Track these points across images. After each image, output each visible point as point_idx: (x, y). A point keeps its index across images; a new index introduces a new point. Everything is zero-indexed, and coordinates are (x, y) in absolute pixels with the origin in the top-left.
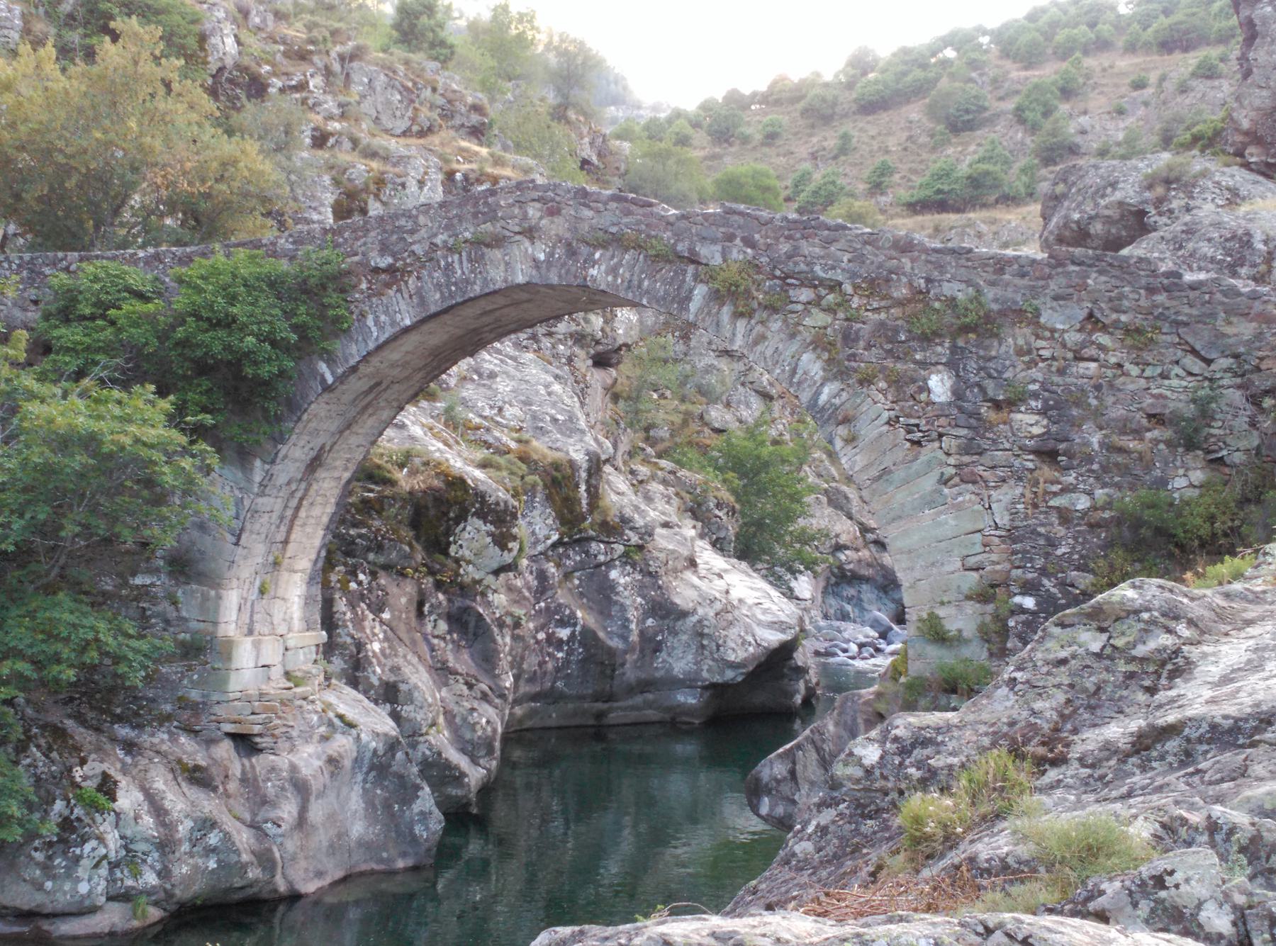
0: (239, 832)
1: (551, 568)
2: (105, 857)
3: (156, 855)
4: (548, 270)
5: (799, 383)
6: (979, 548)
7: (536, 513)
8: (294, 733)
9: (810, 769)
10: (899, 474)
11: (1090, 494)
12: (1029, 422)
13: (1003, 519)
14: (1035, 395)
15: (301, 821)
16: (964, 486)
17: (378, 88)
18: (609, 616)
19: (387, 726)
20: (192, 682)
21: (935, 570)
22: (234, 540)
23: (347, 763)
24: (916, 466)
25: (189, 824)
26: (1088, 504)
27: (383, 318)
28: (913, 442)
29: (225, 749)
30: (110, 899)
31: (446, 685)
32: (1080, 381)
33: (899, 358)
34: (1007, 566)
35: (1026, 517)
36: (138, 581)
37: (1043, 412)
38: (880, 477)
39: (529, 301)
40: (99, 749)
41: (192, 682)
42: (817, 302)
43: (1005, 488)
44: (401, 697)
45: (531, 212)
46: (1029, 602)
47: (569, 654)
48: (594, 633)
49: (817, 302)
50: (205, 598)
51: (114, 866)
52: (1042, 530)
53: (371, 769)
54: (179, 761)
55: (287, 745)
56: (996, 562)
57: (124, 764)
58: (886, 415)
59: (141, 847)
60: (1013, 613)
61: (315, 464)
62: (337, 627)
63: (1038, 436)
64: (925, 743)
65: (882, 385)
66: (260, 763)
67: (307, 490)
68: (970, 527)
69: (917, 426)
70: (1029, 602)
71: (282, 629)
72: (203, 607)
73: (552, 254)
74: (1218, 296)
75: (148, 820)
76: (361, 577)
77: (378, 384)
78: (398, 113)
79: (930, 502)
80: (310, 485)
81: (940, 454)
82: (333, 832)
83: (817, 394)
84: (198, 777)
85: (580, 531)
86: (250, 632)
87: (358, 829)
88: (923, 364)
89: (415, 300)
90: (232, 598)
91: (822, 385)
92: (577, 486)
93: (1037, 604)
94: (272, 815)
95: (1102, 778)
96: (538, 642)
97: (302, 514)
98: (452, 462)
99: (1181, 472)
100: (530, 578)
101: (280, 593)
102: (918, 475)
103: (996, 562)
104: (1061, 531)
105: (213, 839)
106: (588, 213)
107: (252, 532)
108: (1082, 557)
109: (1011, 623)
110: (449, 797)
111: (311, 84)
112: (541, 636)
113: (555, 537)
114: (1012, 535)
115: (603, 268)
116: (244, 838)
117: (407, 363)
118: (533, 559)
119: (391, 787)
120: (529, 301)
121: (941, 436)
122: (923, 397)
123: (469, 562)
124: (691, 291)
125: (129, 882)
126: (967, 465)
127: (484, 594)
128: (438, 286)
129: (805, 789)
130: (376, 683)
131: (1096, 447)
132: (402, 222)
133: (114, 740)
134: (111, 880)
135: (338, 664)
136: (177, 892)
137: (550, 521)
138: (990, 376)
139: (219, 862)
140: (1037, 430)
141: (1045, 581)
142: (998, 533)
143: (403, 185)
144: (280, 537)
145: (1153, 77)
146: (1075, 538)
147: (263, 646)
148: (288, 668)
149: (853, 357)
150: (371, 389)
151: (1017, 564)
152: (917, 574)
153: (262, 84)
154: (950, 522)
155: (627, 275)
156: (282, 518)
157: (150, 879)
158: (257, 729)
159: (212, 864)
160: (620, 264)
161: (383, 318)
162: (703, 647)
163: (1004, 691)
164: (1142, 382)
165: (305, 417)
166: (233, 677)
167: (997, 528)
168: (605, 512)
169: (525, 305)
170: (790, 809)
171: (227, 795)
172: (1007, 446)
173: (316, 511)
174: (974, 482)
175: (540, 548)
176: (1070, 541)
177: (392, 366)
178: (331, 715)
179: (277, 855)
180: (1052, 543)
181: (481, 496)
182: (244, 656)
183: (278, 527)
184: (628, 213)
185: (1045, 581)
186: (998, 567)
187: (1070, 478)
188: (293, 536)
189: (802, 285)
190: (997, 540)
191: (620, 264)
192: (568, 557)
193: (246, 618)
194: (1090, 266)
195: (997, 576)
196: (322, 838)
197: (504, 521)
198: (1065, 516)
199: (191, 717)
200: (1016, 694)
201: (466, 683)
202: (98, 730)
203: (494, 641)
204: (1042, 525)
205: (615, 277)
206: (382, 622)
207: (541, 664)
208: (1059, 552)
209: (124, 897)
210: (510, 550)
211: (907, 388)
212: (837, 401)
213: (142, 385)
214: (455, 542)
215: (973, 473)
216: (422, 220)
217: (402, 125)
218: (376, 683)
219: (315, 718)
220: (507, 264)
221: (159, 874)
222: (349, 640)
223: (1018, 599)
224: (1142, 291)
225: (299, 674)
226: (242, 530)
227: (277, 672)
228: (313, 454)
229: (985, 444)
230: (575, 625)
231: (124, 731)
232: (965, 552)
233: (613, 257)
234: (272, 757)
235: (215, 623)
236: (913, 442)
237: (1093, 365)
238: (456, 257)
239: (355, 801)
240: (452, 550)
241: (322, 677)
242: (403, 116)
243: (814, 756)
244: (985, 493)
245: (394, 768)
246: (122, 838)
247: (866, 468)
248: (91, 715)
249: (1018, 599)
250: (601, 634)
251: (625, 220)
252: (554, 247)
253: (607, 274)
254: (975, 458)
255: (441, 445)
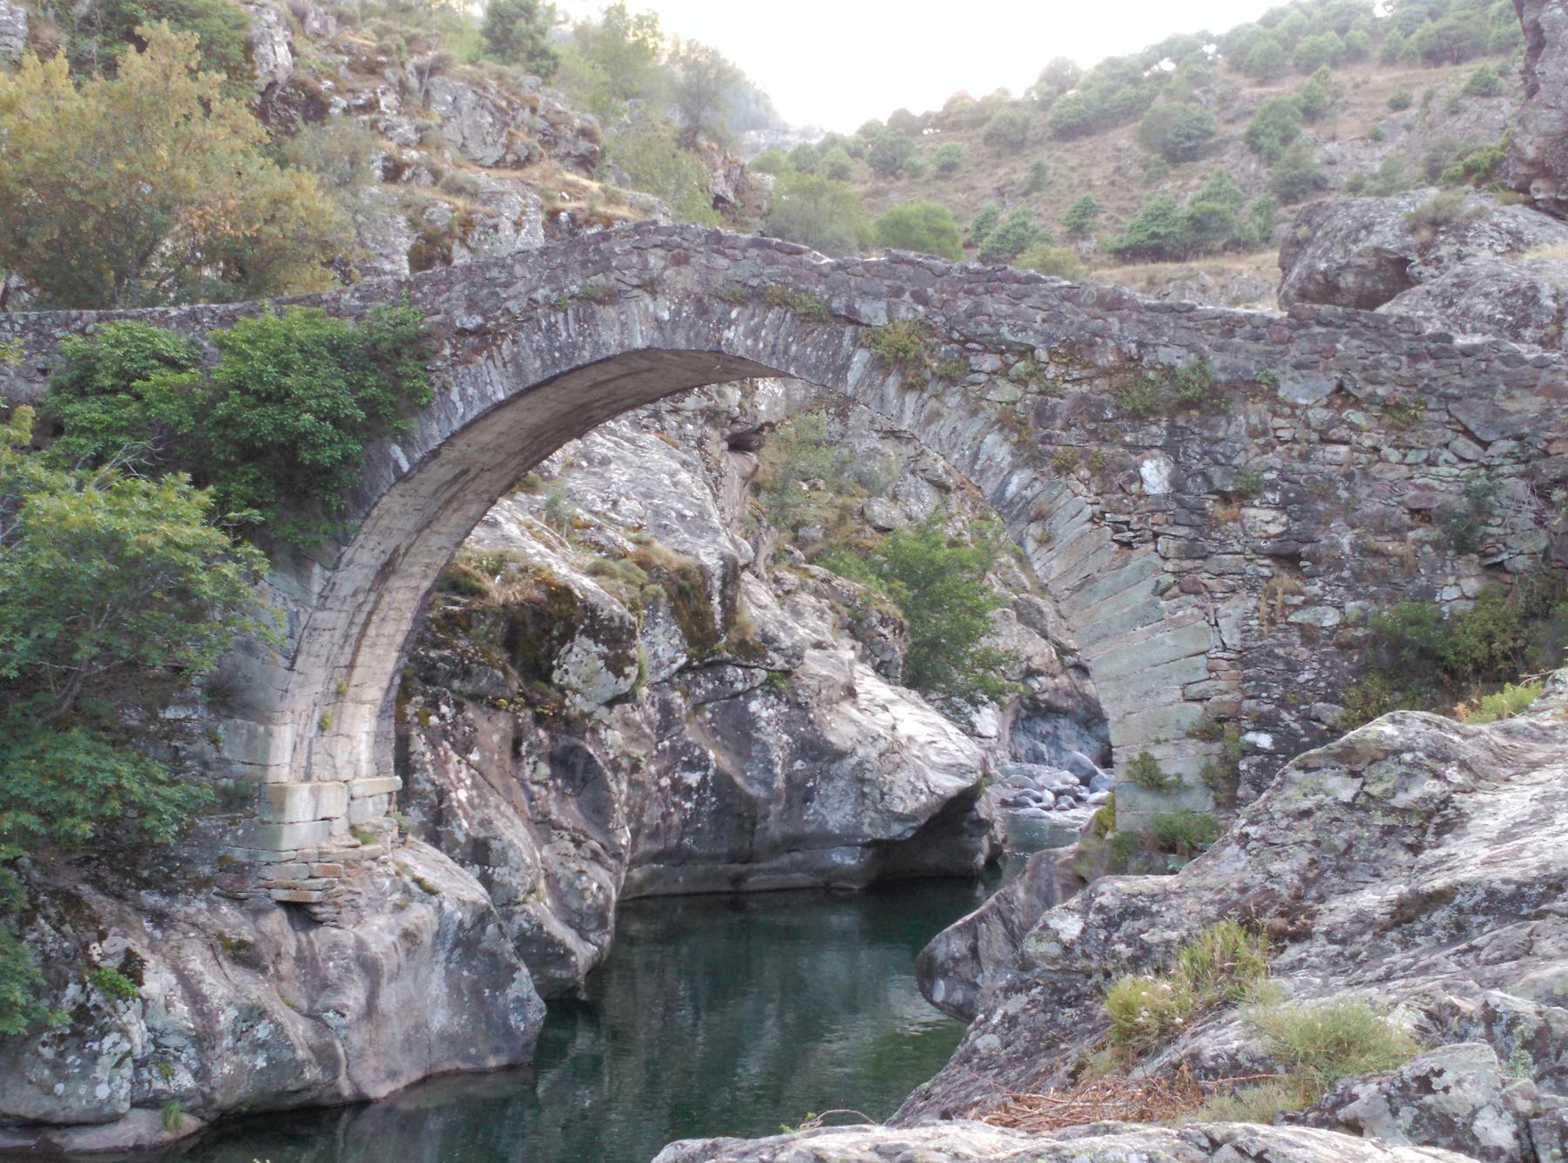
0: (293, 1023)
1: (677, 699)
2: (129, 1053)
3: (192, 1051)
4: (674, 332)
5: (982, 471)
6: (1203, 674)
7: (659, 630)
8: (362, 902)
9: (995, 946)
10: (1105, 583)
11: (1339, 607)
12: (1264, 519)
13: (1233, 639)
14: (1272, 486)
15: (370, 1010)
16: (1184, 597)
17: (465, 109)
18: (749, 757)
19: (476, 892)
20: (236, 838)
21: (1148, 701)
22: (287, 663)
23: (427, 938)
24: (1126, 573)
25: (232, 1013)
26: (1337, 620)
27: (470, 391)
28: (1122, 544)
29: (276, 921)
30: (135, 1105)
31: (548, 842)
32: (1328, 469)
33: (1104, 440)
34: (1238, 695)
35: (1261, 636)
36: (170, 714)
37: (1282, 507)
38: (1081, 586)
39: (650, 370)
40: (121, 921)
41: (236, 838)
42: (1004, 371)
43: (1235, 600)
44: (493, 857)
45: (652, 261)
46: (1265, 741)
47: (699, 803)
48: (730, 778)
49: (1004, 371)
50: (252, 735)
51: (140, 1064)
52: (1280, 651)
53: (456, 945)
54: (220, 936)
55: (353, 916)
56: (1225, 691)
57: (152, 939)
58: (1088, 510)
59: (173, 1041)
60: (1244, 753)
61: (387, 570)
62: (414, 770)
63: (1276, 536)
64: (1137, 913)
65: (1084, 473)
66: (320, 938)
67: (377, 603)
68: (1192, 648)
69: (1127, 523)
70: (1265, 741)
71: (346, 774)
72: (249, 746)
73: (678, 313)
74: (1497, 364)
75: (182, 1009)
76: (444, 709)
77: (465, 472)
78: (489, 139)
79: (1143, 617)
80: (381, 596)
81: (1155, 558)
82: (409, 1023)
83: (1005, 484)
84: (243, 955)
85: (713, 653)
86: (308, 777)
87: (439, 1019)
88: (1135, 448)
89: (510, 369)
90: (285, 736)
91: (1010, 473)
92: (709, 597)
93: (1275, 743)
94: (335, 1002)
95: (1354, 956)
96: (661, 789)
97: (372, 631)
98: (555, 568)
99: (1451, 580)
100: (651, 711)
101: (344, 729)
102: (1128, 585)
103: (1225, 691)
104: (1303, 653)
105: (262, 1031)
106: (722, 262)
107: (309, 654)
108: (1329, 685)
109: (1243, 766)
110: (552, 980)
111: (382, 104)
112: (665, 782)
113: (682, 660)
114: (1243, 658)
115: (741, 329)
116: (299, 1030)
117: (500, 446)
118: (655, 687)
119: (481, 968)
120: (650, 370)
121: (1156, 535)
122: (1134, 488)
123: (576, 691)
124: (849, 357)
125: (159, 1085)
126: (1188, 572)
127: (594, 731)
128: (539, 352)
129: (989, 969)
130: (462, 839)
131: (1347, 549)
132: (494, 273)
133: (140, 909)
134: (137, 1082)
135: (415, 816)
136: (218, 1096)
137: (676, 641)
138: (1217, 463)
139: (269, 1059)
140: (1274, 529)
141: (1284, 715)
142: (1226, 655)
143: (496, 228)
144: (344, 660)
145: (1417, 95)
146: (1321, 662)
147: (323, 794)
148: (354, 822)
149: (1048, 439)
150: (456, 478)
151: (1250, 693)
152: (1127, 706)
153: (322, 103)
154: (1167, 642)
155: (771, 338)
156: (346, 637)
157: (185, 1080)
158: (315, 896)
159: (261, 1063)
160: (761, 325)
161: (470, 391)
162: (864, 795)
163: (1234, 849)
164: (1404, 470)
165: (375, 512)
166: (287, 832)
167: (1225, 649)
168: (743, 630)
169: (646, 375)
170: (971, 994)
171: (279, 977)
172: (1238, 548)
173: (389, 628)
174: (1197, 593)
175: (664, 674)
176: (1315, 665)
177: (482, 450)
178: (407, 879)
179: (341, 1051)
180: (1293, 667)
181: (591, 610)
182: (300, 806)
183: (342, 648)
184: (772, 262)
185: (1284, 715)
186: (1227, 697)
187: (1315, 588)
188: (360, 660)
189: (986, 350)
190: (1225, 664)
191: (761, 325)
192: (698, 685)
193: (302, 760)
194: (1339, 327)
195: (1225, 709)
196: (396, 1030)
197: (619, 641)
198: (1309, 635)
199: (235, 881)
200: (1248, 853)
201: (573, 840)
202: (120, 897)
203: (608, 788)
204: (1281, 645)
205: (756, 341)
206: (469, 765)
207: (665, 816)
208: (1302, 679)
209: (153, 1102)
210: (627, 677)
211: (1114, 477)
212: (1028, 493)
213: (175, 473)
214: (560, 667)
215: (1195, 582)
216: (518, 270)
217: (494, 154)
218: (462, 839)
219: (388, 883)
220: (623, 324)
221: (195, 1075)
222: (429, 787)
223: (1250, 737)
224: (1403, 358)
225: (367, 829)
226: (297, 651)
227: (340, 827)
228: (384, 558)
229: (1210, 546)
230: (707, 768)
231: (152, 899)
232: (1186, 679)
233: (753, 316)
234: (335, 931)
235: (265, 766)
236: (1122, 544)
237: (1343, 449)
238: (561, 316)
239: (437, 985)
240: (556, 676)
241: (395, 833)
242: (495, 143)
243: (1001, 929)
244: (1210, 606)
245: (485, 944)
246: (149, 1030)
247: (1064, 575)
248: (111, 879)
249: (1250, 737)
250: (739, 780)
251: (768, 271)
252: (681, 304)
253: (746, 337)
254: (1198, 563)
255: (541, 548)
